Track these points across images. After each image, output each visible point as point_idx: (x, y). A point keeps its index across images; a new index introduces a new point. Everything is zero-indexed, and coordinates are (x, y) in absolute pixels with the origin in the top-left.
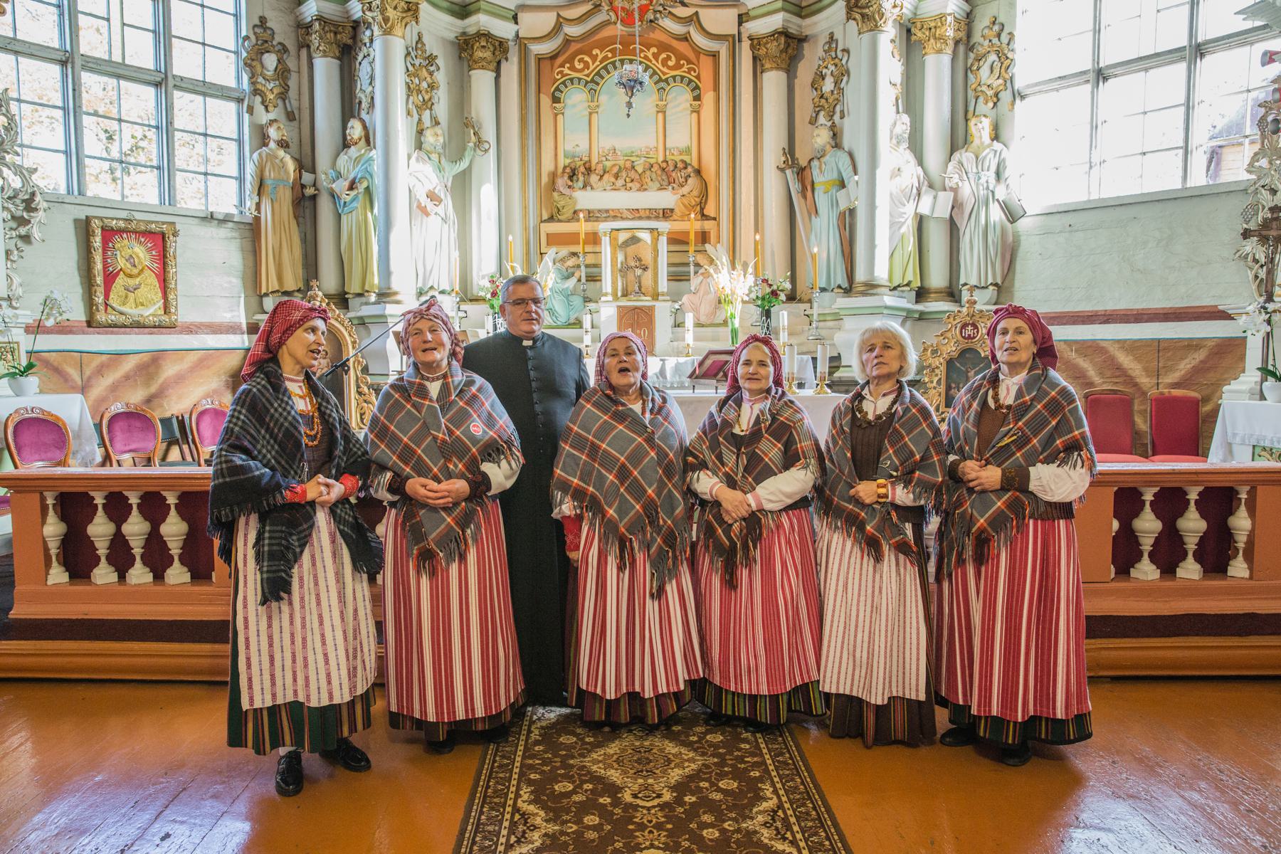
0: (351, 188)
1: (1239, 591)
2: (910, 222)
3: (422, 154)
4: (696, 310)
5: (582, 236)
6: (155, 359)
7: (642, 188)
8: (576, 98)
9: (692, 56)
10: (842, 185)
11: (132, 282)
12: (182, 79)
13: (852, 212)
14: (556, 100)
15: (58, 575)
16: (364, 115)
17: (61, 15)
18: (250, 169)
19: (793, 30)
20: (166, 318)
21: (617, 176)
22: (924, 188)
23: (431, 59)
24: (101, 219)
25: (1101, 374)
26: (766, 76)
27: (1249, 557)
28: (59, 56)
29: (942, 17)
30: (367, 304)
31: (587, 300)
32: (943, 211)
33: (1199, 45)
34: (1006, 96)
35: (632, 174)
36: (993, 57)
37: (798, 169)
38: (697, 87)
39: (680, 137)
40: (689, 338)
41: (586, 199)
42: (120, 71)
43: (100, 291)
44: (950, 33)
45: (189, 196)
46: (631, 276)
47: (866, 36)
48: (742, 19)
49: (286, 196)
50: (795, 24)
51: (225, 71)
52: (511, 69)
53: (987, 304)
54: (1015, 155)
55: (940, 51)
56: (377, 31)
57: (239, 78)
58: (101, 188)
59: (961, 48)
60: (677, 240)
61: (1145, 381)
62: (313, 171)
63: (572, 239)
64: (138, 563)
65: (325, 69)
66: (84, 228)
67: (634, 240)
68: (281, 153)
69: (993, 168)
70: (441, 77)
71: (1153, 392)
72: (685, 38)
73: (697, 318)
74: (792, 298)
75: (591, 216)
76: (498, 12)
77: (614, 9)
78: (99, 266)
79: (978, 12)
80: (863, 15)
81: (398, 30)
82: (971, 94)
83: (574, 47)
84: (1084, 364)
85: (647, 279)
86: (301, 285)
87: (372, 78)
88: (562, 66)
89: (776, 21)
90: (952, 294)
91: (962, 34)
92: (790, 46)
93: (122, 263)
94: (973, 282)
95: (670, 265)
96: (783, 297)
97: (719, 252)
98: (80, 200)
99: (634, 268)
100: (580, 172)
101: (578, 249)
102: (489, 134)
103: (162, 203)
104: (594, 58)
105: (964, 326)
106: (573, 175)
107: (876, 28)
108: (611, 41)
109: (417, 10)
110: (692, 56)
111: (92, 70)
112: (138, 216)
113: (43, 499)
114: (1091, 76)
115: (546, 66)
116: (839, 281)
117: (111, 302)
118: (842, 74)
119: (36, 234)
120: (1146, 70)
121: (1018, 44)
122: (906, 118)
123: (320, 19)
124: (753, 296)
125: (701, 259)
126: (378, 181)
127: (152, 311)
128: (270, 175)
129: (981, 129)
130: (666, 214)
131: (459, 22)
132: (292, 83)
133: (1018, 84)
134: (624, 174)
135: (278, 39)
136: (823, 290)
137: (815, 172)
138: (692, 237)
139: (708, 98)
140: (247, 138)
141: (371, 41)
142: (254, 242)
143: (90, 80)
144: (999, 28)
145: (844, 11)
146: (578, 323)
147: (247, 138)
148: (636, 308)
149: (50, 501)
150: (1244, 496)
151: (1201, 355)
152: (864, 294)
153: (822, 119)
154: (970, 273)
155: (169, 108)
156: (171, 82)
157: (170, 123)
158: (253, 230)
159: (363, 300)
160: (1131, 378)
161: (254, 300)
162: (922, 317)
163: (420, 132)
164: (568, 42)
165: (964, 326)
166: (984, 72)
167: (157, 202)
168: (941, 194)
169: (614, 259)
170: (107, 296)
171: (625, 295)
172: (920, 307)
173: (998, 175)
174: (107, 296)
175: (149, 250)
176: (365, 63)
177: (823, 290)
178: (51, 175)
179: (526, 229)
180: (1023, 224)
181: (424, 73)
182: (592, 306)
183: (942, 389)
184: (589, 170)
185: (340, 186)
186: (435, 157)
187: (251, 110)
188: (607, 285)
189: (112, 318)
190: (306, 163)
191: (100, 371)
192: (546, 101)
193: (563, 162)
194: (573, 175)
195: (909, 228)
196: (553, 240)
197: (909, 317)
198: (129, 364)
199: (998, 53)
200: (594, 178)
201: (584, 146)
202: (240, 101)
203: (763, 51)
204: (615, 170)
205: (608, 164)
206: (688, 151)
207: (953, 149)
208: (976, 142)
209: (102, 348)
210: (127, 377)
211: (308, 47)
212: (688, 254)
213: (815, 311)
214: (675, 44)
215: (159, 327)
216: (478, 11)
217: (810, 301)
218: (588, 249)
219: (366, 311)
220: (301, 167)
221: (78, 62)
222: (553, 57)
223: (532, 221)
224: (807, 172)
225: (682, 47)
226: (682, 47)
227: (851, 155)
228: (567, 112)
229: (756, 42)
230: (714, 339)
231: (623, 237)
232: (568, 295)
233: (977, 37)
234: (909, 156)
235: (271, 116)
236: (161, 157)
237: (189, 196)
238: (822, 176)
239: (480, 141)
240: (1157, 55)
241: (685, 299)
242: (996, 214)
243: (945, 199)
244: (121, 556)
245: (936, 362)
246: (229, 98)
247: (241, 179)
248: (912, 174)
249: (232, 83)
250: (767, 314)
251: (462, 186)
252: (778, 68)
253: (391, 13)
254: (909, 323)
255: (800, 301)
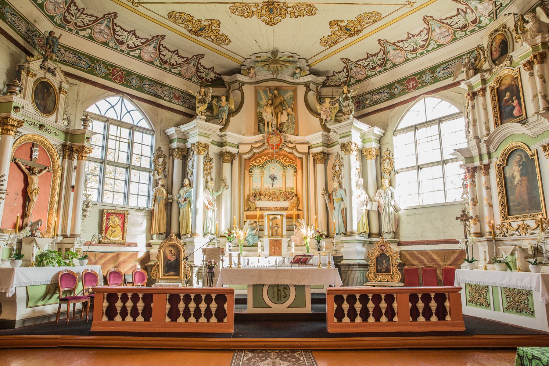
0: (185, 200)
1: (449, 324)
2: (364, 212)
3: (207, 190)
4: (295, 241)
5: (258, 216)
6: (118, 254)
7: (278, 200)
8: (257, 171)
9: (294, 159)
10: (342, 200)
11: (114, 229)
12: (134, 166)
13: (346, 208)
14: (250, 172)
15: (105, 318)
16: (189, 177)
17: (103, 149)
18: (152, 194)
19: (326, 151)
20: (122, 241)
21: (270, 196)
22: (368, 201)
23: (211, 160)
24: (107, 209)
25: (428, 261)
26: (318, 165)
27: (450, 315)
28: (101, 161)
29: (371, 149)
30: (187, 238)
31: (260, 237)
32: (375, 208)
33: (444, 161)
34: (393, 172)
35: (275, 196)
36: (388, 160)
37: (328, 193)
38: (296, 168)
39: (290, 184)
40: (293, 250)
41: (260, 204)
42: (116, 164)
43: (104, 232)
44: (374, 153)
45: (133, 202)
46: (274, 230)
47: (347, 156)
48: (310, 148)
49: (163, 202)
50: (326, 150)
51: (146, 163)
52: (236, 163)
53: (391, 238)
54: (397, 192)
55: (371, 159)
56: (195, 153)
57: (151, 165)
58: (108, 199)
59: (378, 157)
60: (289, 217)
61: (441, 263)
62: (172, 194)
63: (255, 217)
64: (129, 315)
65: (177, 163)
66: (102, 212)
67: (275, 218)
68: (162, 189)
69: (390, 195)
70: (214, 165)
71: (443, 267)
72: (292, 153)
73: (296, 243)
74: (328, 236)
75: (261, 209)
76: (232, 145)
77: (269, 145)
78: (104, 224)
79: (383, 147)
80: (346, 150)
81: (202, 153)
82: (382, 171)
83: (256, 156)
84: (422, 258)
85: (279, 231)
86: (165, 231)
87: (192, 167)
88: (252, 161)
89: (320, 149)
90: (380, 235)
91: (378, 153)
92: (325, 156)
93: (111, 223)
94: (386, 231)
95: (287, 225)
96: (324, 236)
97: (303, 222)
98: (102, 204)
99: (275, 228)
100: (257, 195)
101: (257, 220)
102: (229, 183)
103: (124, 204)
104: (263, 159)
105: (381, 246)
106: (255, 196)
107: (350, 153)
108: (268, 154)
109: (208, 147)
110: (294, 159)
111: (109, 165)
112: (118, 209)
113: (104, 295)
114: (416, 167)
115: (247, 161)
116: (343, 231)
117: (107, 236)
118: (341, 165)
119: (88, 214)
120: (432, 167)
121: (395, 157)
122: (361, 179)
123: (178, 148)
124: (314, 236)
125: (297, 224)
126: (193, 198)
127: (118, 239)
128: (158, 195)
129: (386, 182)
130: (286, 209)
131: (220, 148)
132: (167, 166)
133: (396, 169)
134: (272, 196)
135: (163, 153)
136: (337, 234)
137: (334, 196)
138: (294, 216)
139: (299, 172)
140: (152, 183)
141: (193, 154)
142: (151, 217)
143: (109, 168)
144: (389, 152)
145: (340, 148)
146: (256, 245)
147: (152, 183)
148: (276, 240)
149: (105, 296)
150: (447, 296)
151: (456, 255)
152: (350, 236)
153: (336, 179)
154: (385, 229)
155: (130, 175)
156: (131, 167)
157: (129, 180)
158: (151, 214)
159: (186, 236)
160: (437, 262)
161: (150, 236)
162: (370, 243)
163: (207, 182)
164: (254, 154)
165: (381, 246)
166: (386, 165)
167: (122, 204)
168: (374, 203)
169: (268, 224)
170: (106, 234)
171: (272, 236)
172: (369, 240)
173: (392, 197)
174: (106, 234)
175: (120, 219)
176: (190, 161)
177: (337, 234)
178: (94, 198)
179: (240, 213)
180: (400, 213)
181: (209, 164)
182: (261, 239)
183: (375, 267)
184: (261, 194)
185: (181, 200)
186: (211, 190)
187: (154, 175)
188: (266, 232)
189: (107, 241)
190: (170, 191)
191: (101, 258)
192: (247, 172)
193: (252, 191)
194: (255, 196)
195: (364, 213)
196: (248, 217)
197: (365, 243)
198: (110, 256)
199: (389, 159)
200: (262, 197)
201: (259, 187)
202: (150, 172)
203: (316, 158)
204: (269, 194)
205: (267, 192)
206: (293, 188)
207: (378, 188)
208: (384, 187)
209: (102, 250)
210: (108, 260)
211: (173, 156)
212: (293, 221)
213: (335, 241)
214: (289, 155)
215: (120, 244)
216: (226, 145)
217: (333, 238)
218: (260, 220)
219: (187, 240)
220: (168, 193)
221: (106, 163)
222: (250, 159)
223: (242, 211)
224: (331, 196)
225: (291, 156)
226: (291, 156)
227: (345, 191)
228: (254, 176)
229: (314, 155)
230: (302, 251)
231: (271, 217)
232: (253, 236)
233: (383, 154)
234: (364, 192)
235: (160, 177)
236: (125, 190)
237: (133, 202)
238: (336, 197)
239: (225, 185)
240: (434, 163)
241: (292, 237)
242: (392, 210)
243: (375, 205)
244: (124, 313)
245: (373, 258)
246: (147, 171)
247: (148, 197)
248: (364, 196)
249: (148, 167)
250: (319, 242)
251: (219, 199)
252: (321, 163)
253: (200, 148)
254: (366, 245)
255: (331, 237)
